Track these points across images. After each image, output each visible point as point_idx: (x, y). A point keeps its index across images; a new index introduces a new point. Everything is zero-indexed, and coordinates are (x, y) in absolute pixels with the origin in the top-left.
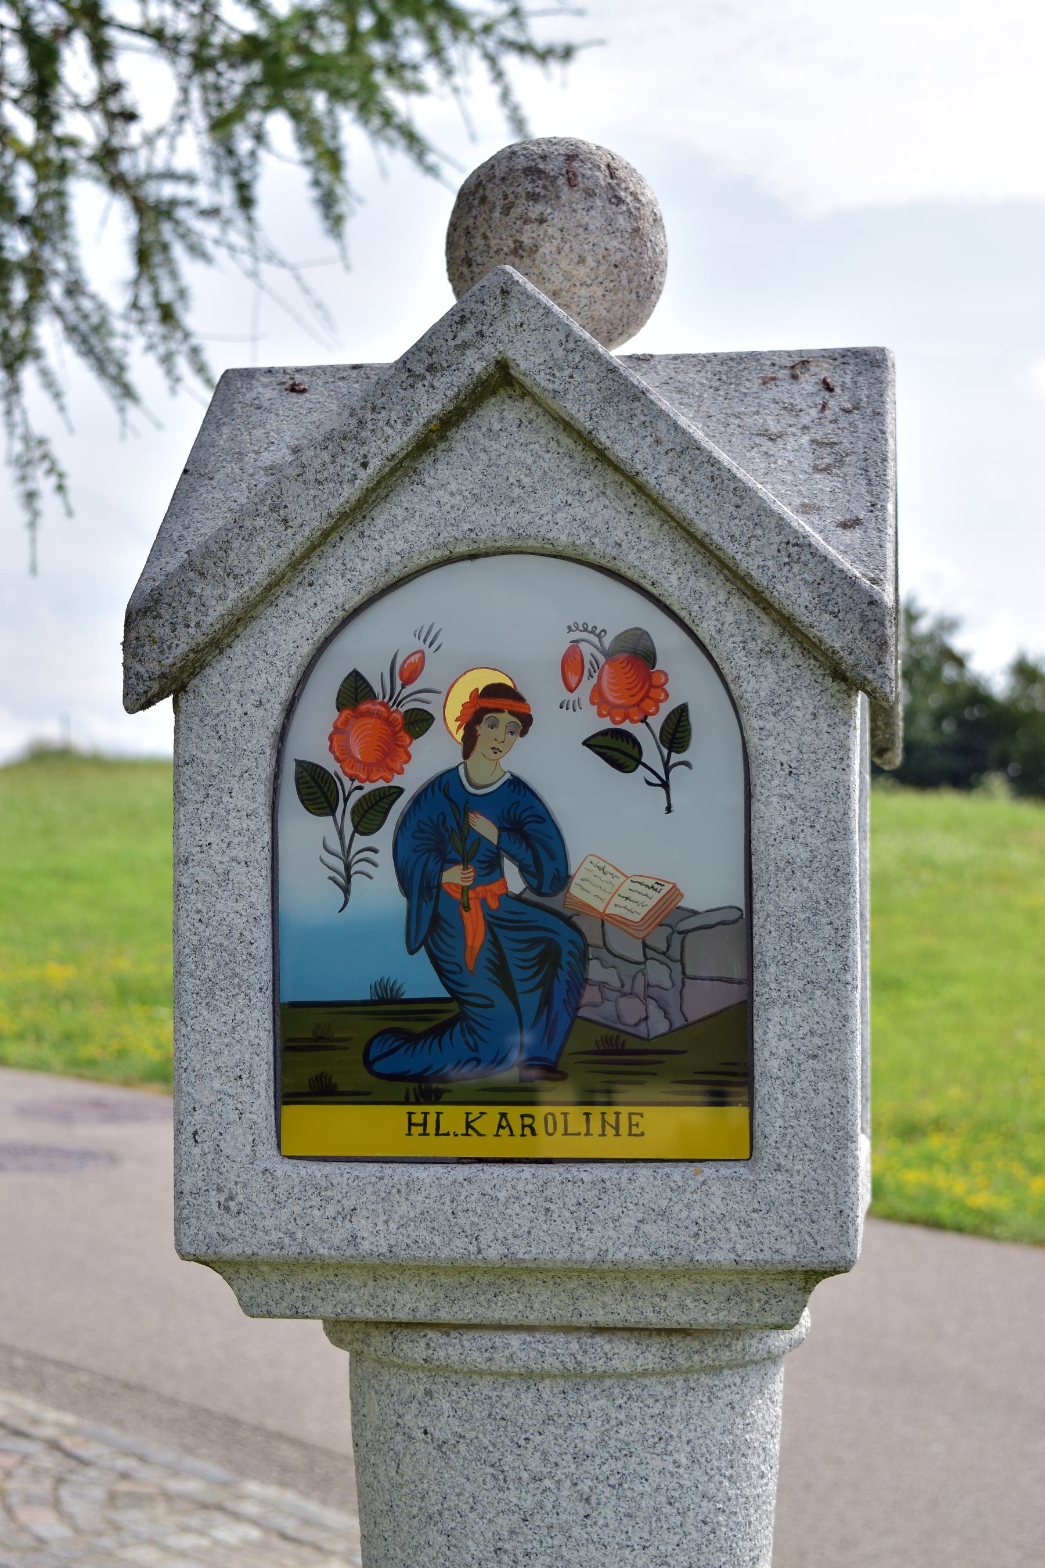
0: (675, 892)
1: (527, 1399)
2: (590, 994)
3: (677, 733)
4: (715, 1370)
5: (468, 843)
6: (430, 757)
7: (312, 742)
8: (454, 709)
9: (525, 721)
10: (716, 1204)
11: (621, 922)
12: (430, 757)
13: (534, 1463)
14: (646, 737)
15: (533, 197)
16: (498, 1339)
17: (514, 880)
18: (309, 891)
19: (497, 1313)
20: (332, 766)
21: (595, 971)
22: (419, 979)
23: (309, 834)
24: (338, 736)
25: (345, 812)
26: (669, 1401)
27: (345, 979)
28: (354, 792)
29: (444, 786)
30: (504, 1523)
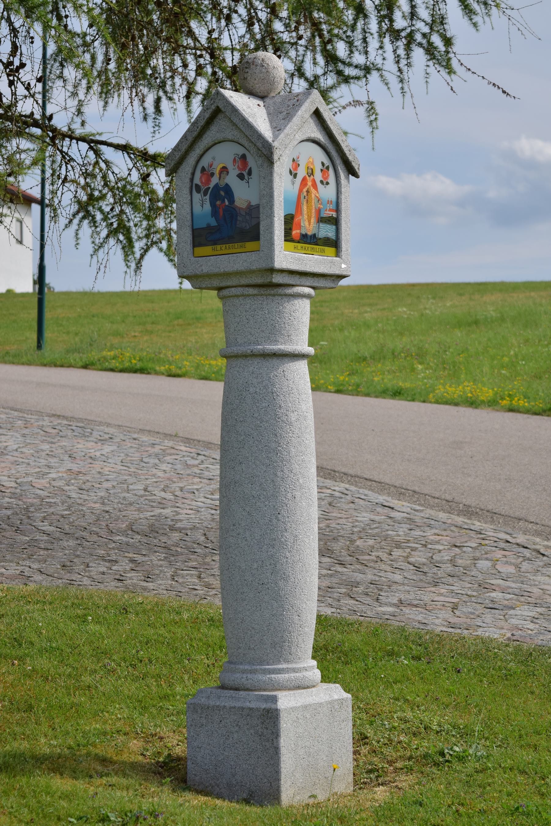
0: (250, 202)
1: (237, 301)
2: (238, 222)
3: (250, 173)
4: (274, 295)
5: (221, 195)
6: (215, 180)
7: (197, 180)
8: (218, 172)
9: (228, 172)
10: (253, 258)
11: (242, 208)
12: (215, 180)
13: (239, 313)
14: (245, 173)
15: (246, 68)
16: (231, 289)
17: (227, 203)
18: (197, 209)
19: (229, 283)
20: (200, 184)
21: (239, 218)
22: (213, 223)
23: (197, 197)
24: (201, 178)
25: (202, 192)
26: (263, 301)
27: (200, 224)
28: (203, 188)
29: (216, 186)
30: (236, 324)
